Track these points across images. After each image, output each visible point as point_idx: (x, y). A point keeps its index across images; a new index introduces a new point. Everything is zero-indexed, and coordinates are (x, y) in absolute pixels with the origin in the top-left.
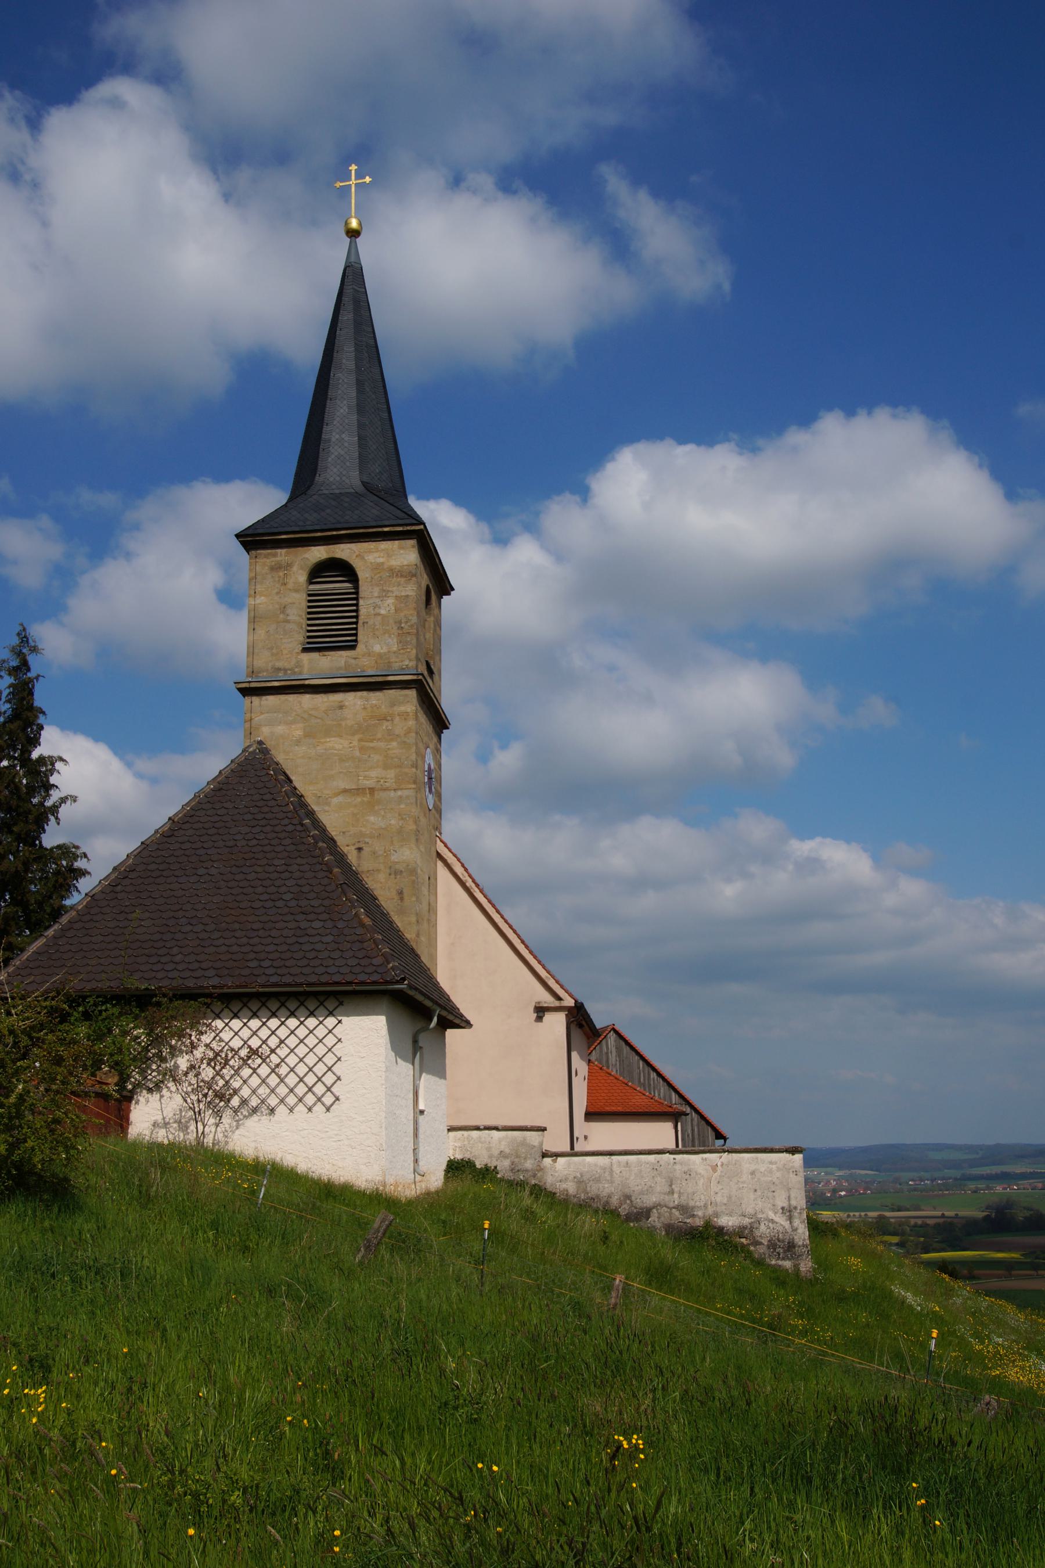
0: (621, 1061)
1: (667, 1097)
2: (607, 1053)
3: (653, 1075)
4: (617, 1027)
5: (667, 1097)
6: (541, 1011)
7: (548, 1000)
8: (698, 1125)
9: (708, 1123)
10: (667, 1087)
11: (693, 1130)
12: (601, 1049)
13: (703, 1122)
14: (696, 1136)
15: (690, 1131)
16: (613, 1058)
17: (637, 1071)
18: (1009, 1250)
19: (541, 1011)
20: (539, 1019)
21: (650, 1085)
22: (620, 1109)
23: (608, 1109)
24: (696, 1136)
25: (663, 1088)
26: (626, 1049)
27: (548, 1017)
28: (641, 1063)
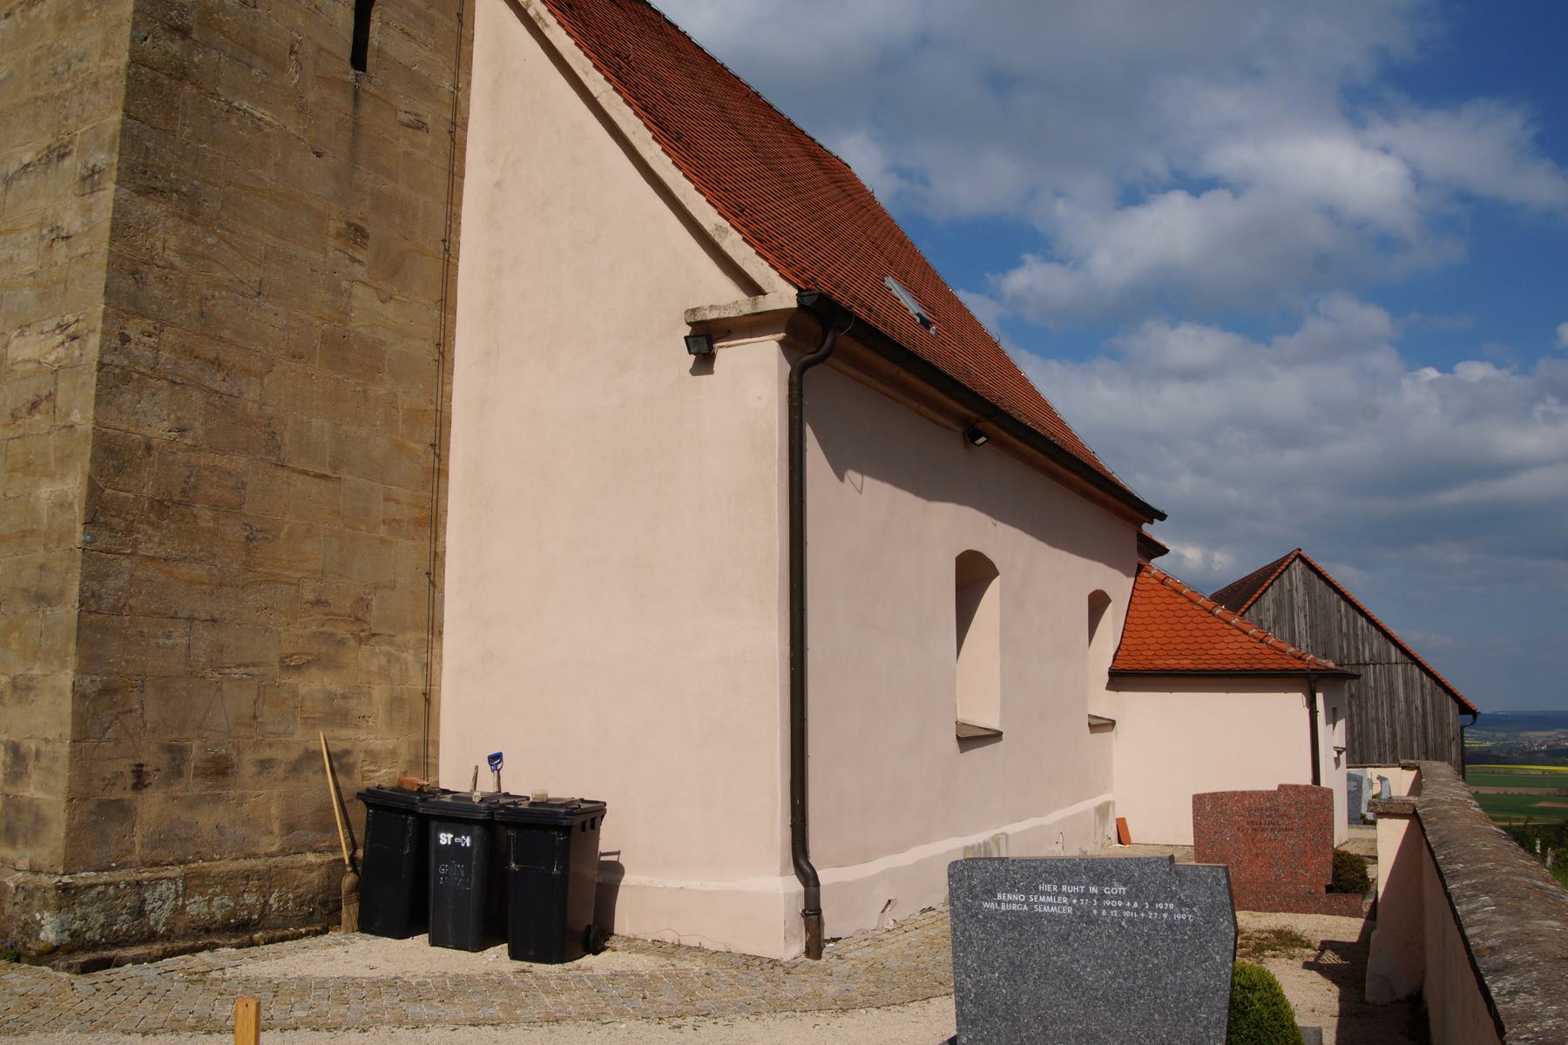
0: (1312, 602)
1: (1384, 654)
2: (1291, 591)
3: (1362, 621)
4: (1304, 553)
5: (1384, 654)
6: (706, 338)
7: (724, 298)
8: (1432, 694)
9: (1448, 691)
10: (1382, 639)
11: (1424, 702)
12: (1281, 587)
13: (1440, 690)
14: (1429, 709)
15: (1419, 703)
16: (1299, 597)
17: (1337, 616)
18: (966, 405)
19: (706, 338)
20: (704, 362)
21: (1356, 635)
22: (1186, 663)
23: (1160, 663)
24: (1429, 709)
25: (1377, 641)
26: (1319, 585)
27: (728, 355)
28: (1343, 604)
